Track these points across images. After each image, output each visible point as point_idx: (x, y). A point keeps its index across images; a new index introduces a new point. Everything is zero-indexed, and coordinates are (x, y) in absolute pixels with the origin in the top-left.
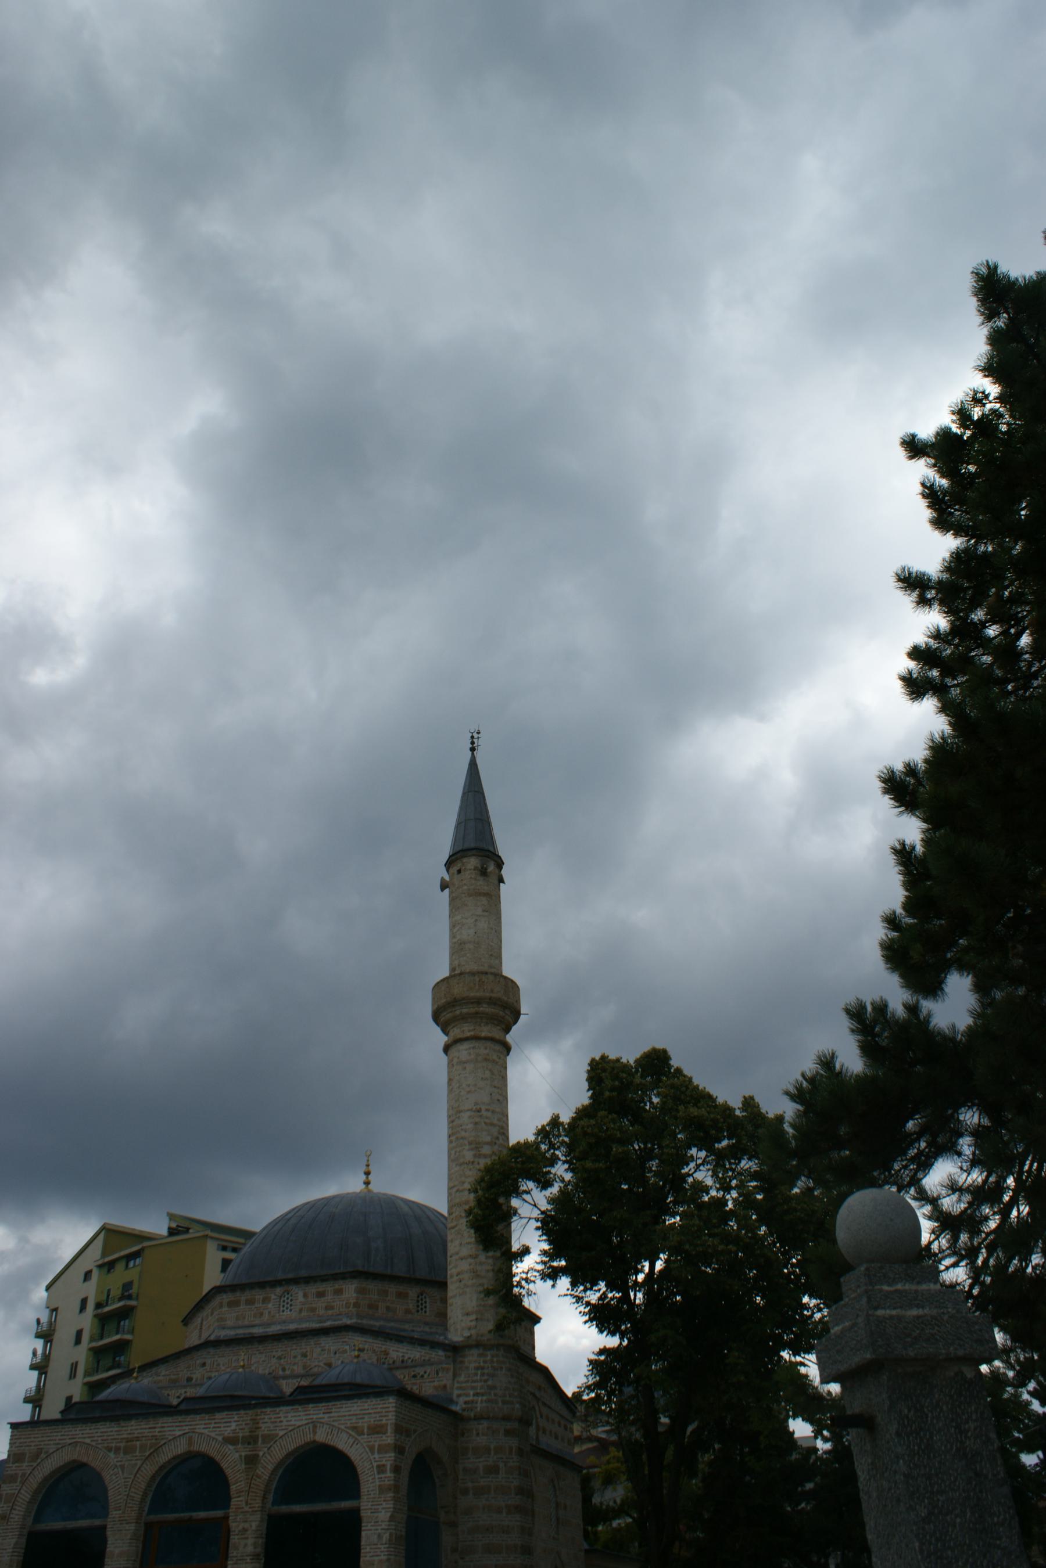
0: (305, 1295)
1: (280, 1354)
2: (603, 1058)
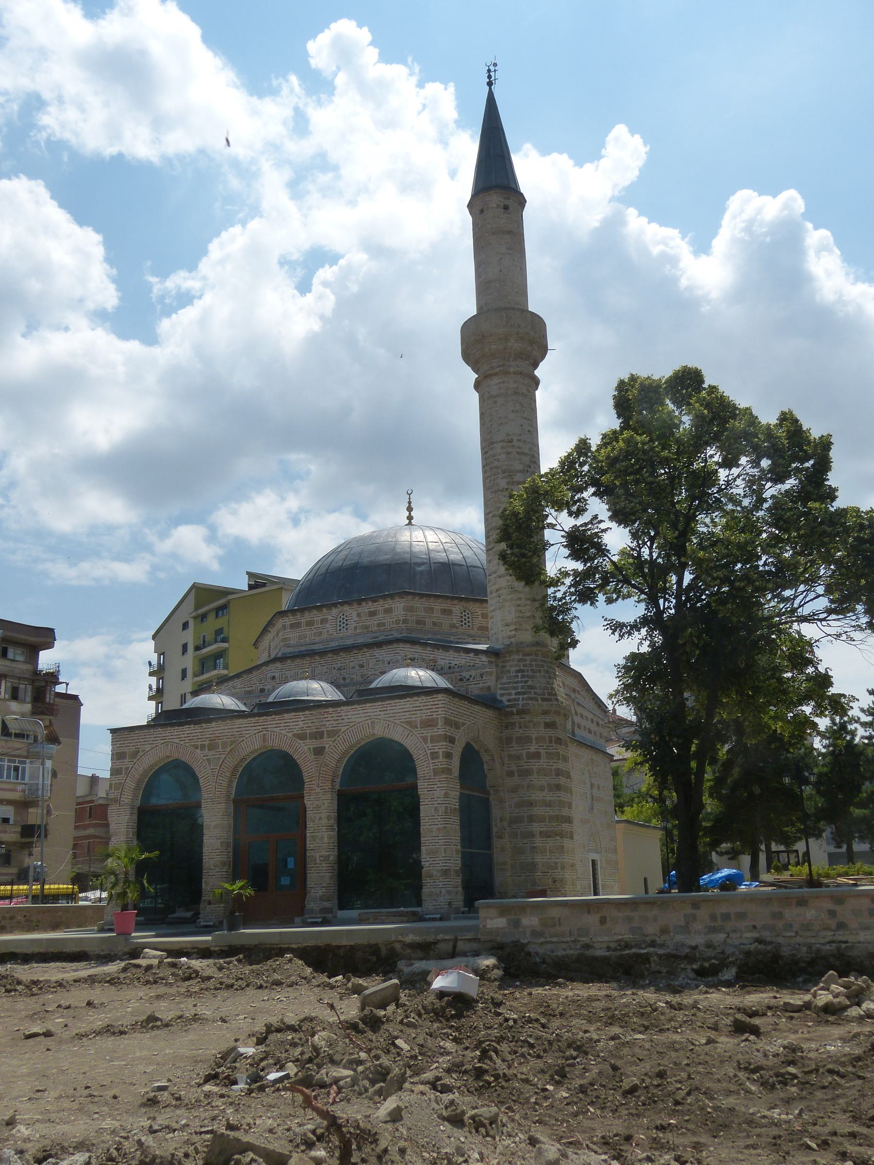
0: (359, 615)
1: (339, 665)
2: (633, 378)
